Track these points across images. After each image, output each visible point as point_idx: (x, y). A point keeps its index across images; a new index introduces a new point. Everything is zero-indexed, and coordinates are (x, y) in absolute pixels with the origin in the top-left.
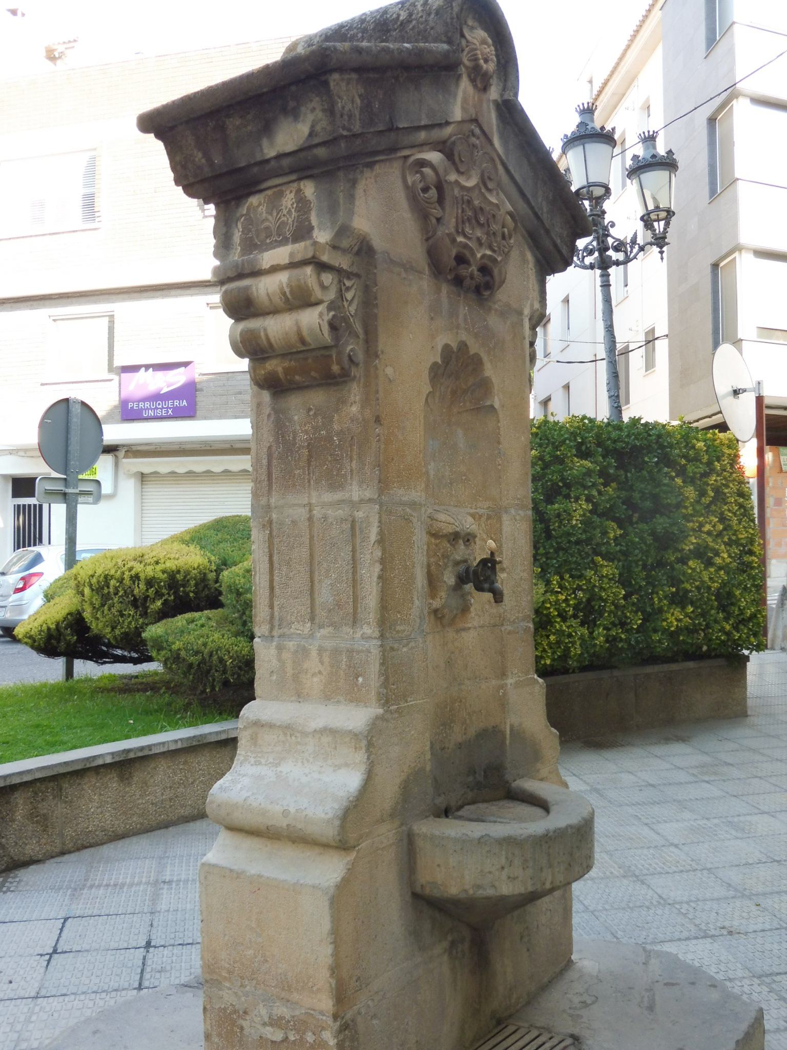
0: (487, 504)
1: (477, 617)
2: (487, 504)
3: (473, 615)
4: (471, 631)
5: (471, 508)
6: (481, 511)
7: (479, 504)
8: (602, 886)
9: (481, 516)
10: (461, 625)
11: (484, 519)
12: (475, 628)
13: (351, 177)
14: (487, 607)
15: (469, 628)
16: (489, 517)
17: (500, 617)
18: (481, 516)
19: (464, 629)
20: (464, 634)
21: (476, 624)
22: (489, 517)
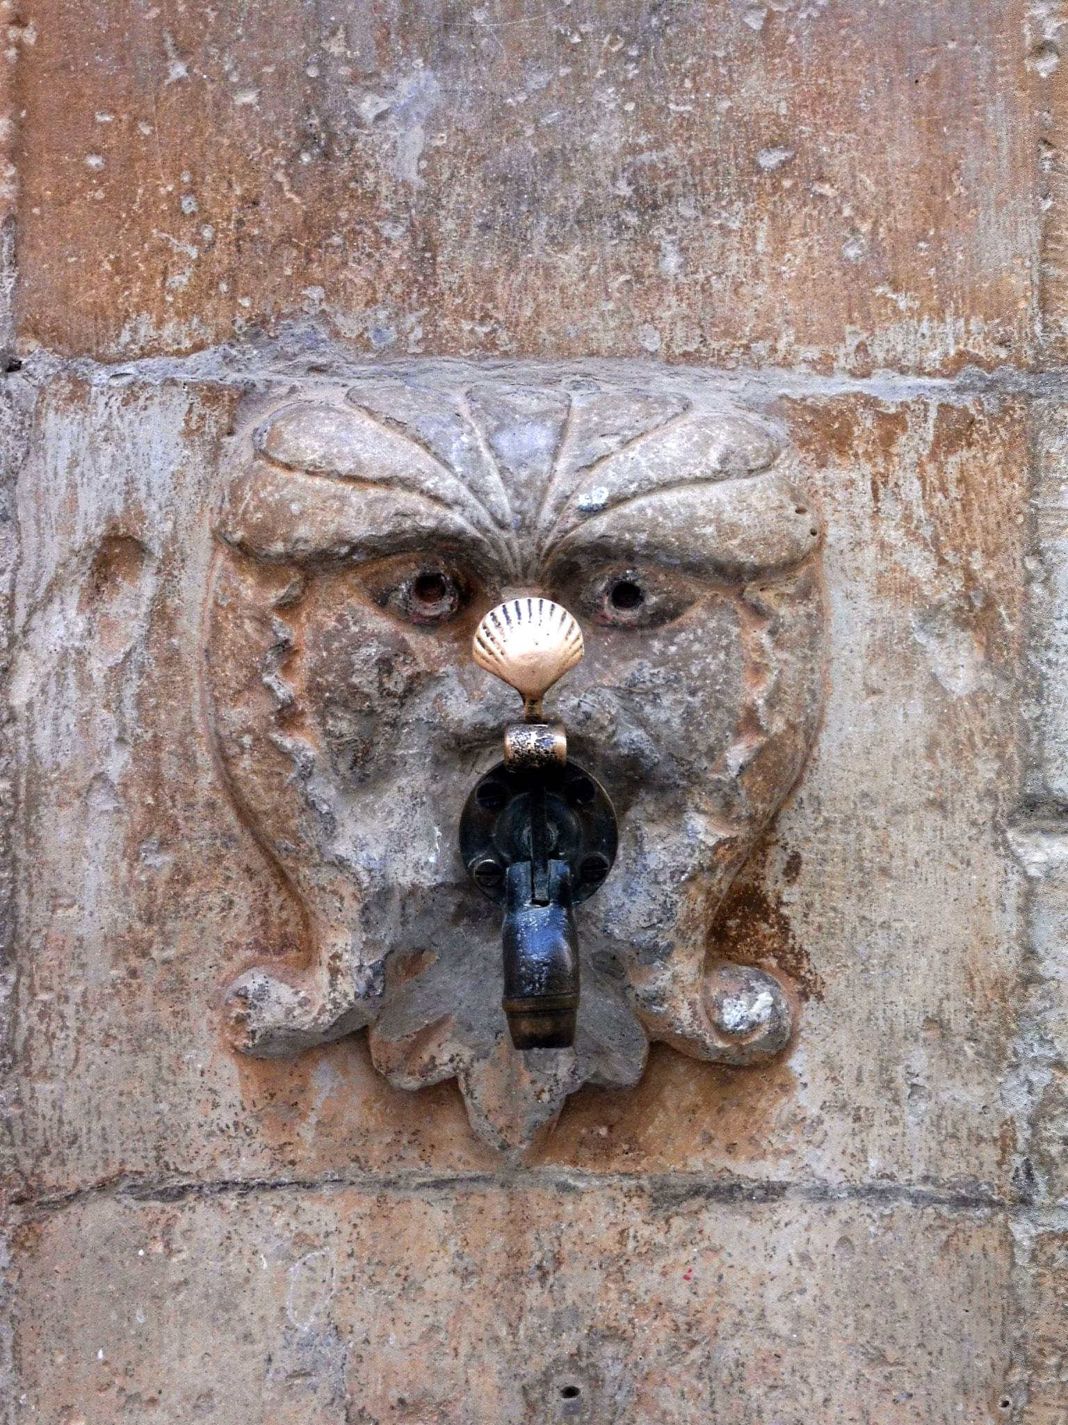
0: (945, 338)
1: (837, 1126)
2: (945, 338)
3: (808, 1100)
4: (788, 1209)
5: (825, 366)
6: (891, 390)
7: (892, 339)
8: (54, 402)
9: (892, 425)
10: (702, 1163)
11: (913, 443)
12: (822, 1194)
13: (778, 1081)
14: (919, 1059)
15: (773, 1192)
16: (956, 432)
17: (1005, 1144)
18: (892, 425)
19: (727, 1192)
20: (719, 1222)
21: (826, 1164)
22: (956, 432)
